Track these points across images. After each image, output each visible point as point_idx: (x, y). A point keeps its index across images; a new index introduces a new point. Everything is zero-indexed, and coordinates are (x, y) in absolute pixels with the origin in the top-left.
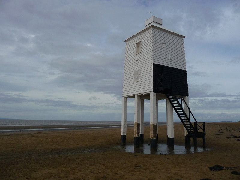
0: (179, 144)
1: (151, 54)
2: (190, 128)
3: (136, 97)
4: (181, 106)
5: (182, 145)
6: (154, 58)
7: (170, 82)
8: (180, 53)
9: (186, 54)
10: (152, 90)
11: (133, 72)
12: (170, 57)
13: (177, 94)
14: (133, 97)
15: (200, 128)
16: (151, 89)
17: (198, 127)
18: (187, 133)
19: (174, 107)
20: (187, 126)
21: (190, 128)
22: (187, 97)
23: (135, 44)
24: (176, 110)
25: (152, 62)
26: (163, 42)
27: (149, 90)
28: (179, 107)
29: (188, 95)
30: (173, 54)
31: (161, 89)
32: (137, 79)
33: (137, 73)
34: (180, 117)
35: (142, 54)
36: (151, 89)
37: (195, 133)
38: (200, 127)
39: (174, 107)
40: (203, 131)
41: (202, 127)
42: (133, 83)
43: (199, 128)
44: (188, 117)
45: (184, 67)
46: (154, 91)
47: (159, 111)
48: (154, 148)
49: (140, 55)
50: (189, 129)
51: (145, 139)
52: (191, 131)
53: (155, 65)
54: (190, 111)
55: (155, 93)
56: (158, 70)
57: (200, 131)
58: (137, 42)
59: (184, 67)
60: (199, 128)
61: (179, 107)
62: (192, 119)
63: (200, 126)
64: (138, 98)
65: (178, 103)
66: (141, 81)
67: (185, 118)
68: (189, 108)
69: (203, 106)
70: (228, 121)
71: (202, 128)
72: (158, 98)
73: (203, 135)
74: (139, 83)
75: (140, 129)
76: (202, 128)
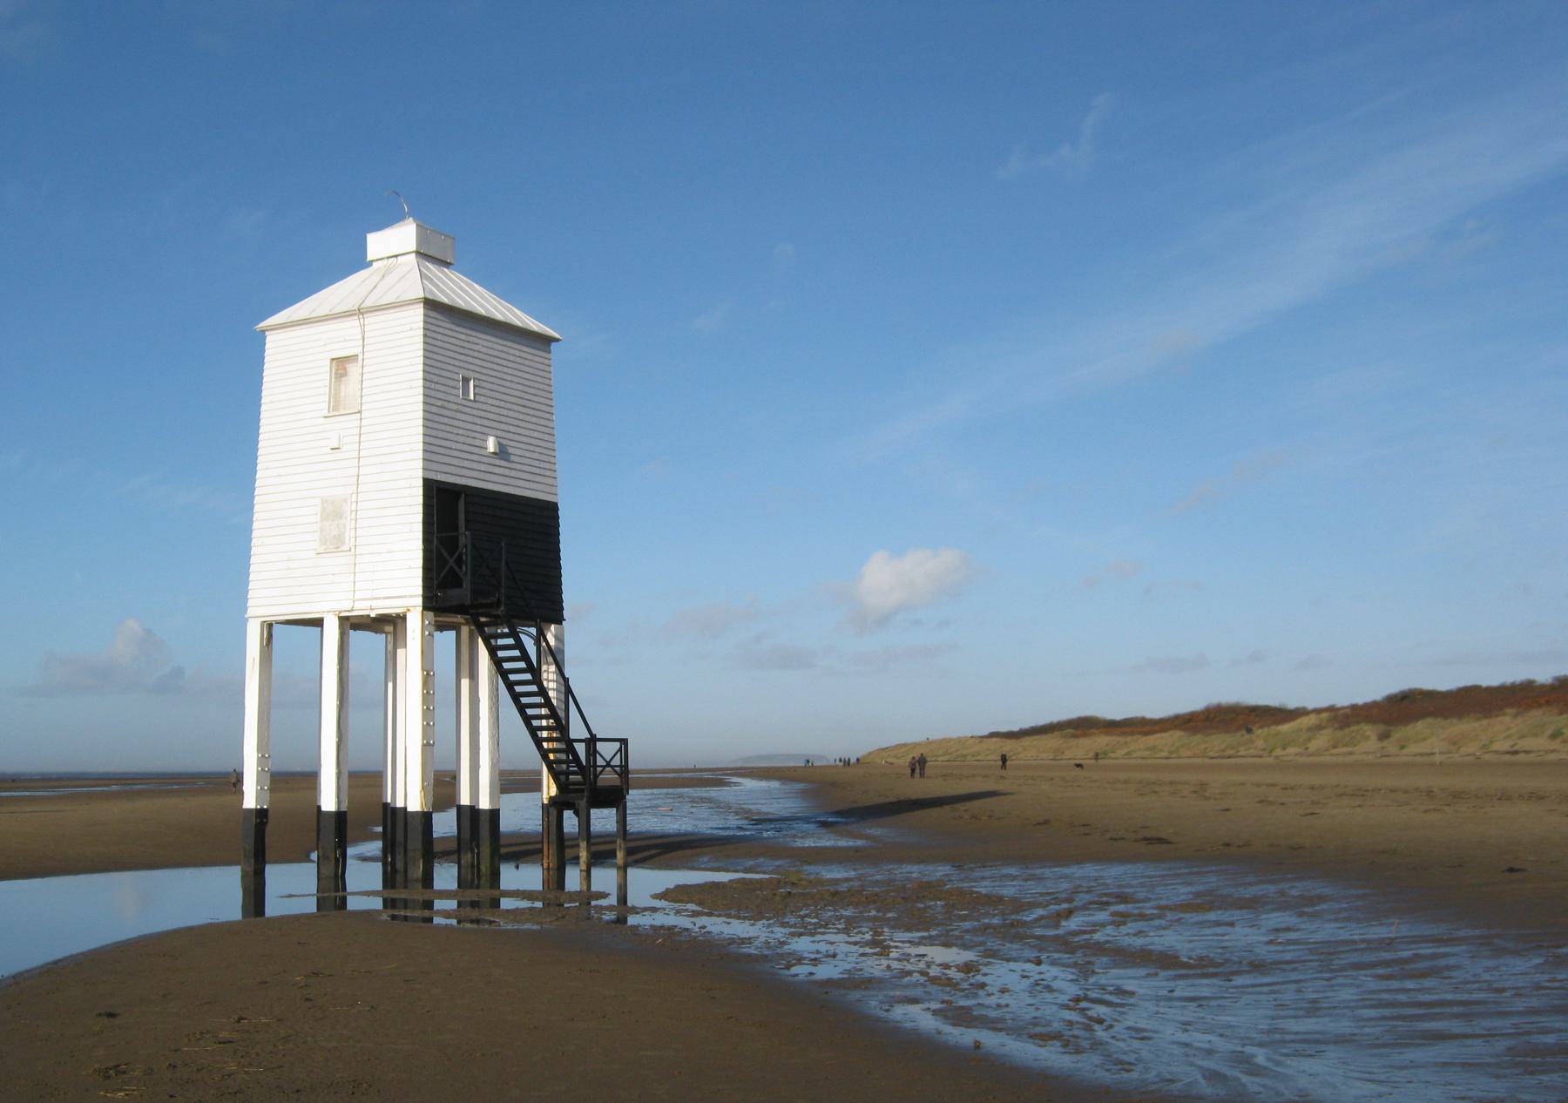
4: (537, 680)
17: (600, 761)
18: (554, 791)
28: (528, 676)
29: (558, 619)
31: (464, 594)
33: (333, 511)
40: (618, 782)
44: (562, 714)
46: (426, 608)
48: (480, 884)
53: (428, 484)
54: (568, 691)
55: (431, 614)
56: (446, 506)
57: (608, 778)
61: (528, 676)
62: (577, 730)
67: (545, 714)
70: (760, 757)
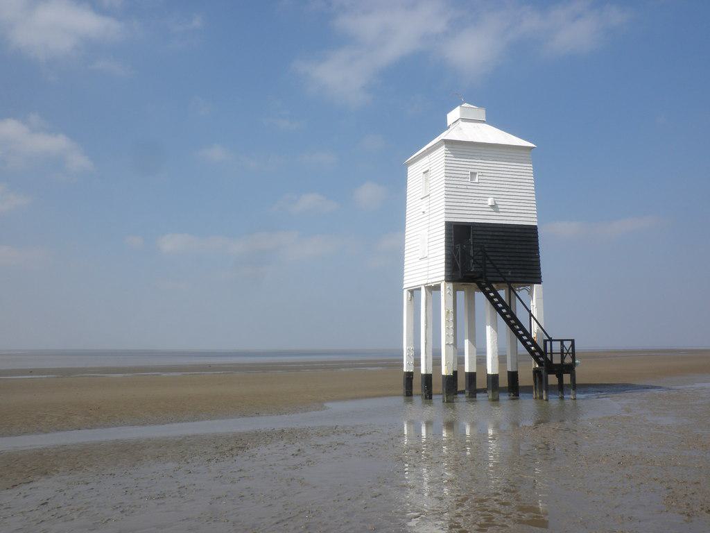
0: (568, 385)
1: (441, 201)
6: (448, 209)
10: (443, 278)
12: (490, 202)
13: (514, 282)
25: (444, 220)
26: (473, 171)
27: (436, 277)
30: (521, 184)
35: (431, 199)
41: (570, 351)
42: (418, 260)
46: (447, 281)
57: (568, 360)
66: (430, 256)
68: (530, 311)
73: (570, 368)
74: (427, 261)
75: (171, 374)
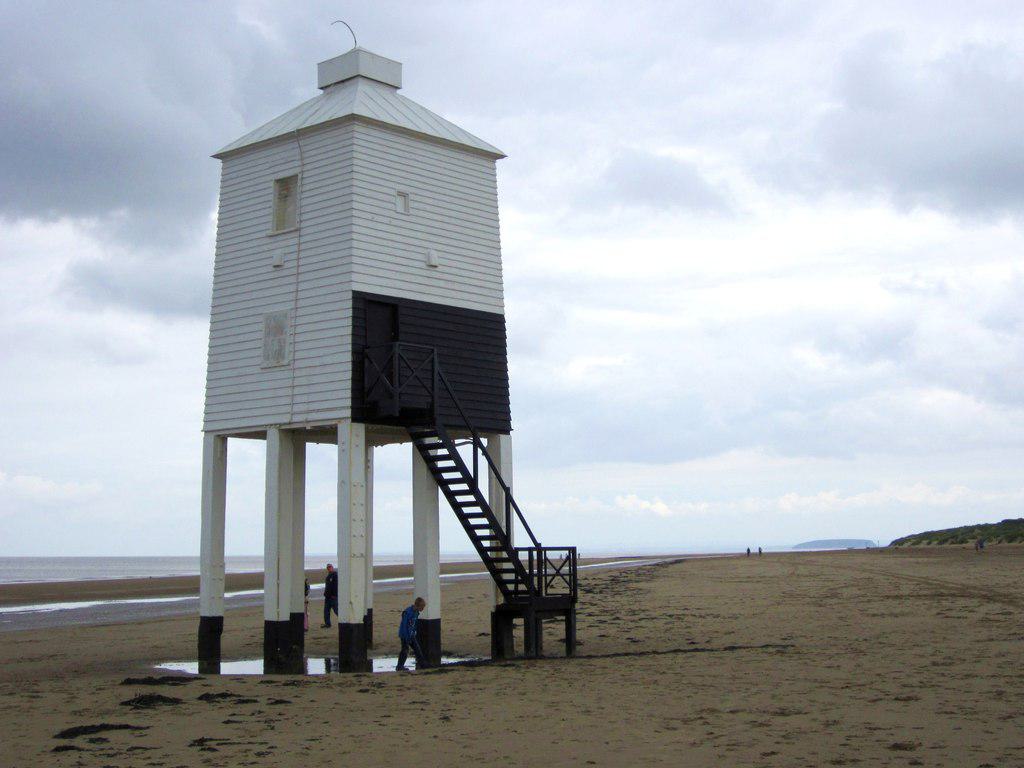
2: (512, 576)
3: (273, 434)
5: (233, 558)
7: (430, 374)
8: (460, 182)
9: (500, 210)
10: (348, 413)
11: (261, 319)
14: (260, 435)
15: (558, 573)
16: (343, 408)
19: (444, 484)
20: (498, 565)
21: (512, 576)
22: (503, 437)
23: (272, 184)
24: (450, 495)
32: (280, 354)
33: (276, 328)
34: (476, 540)
36: (343, 408)
37: (536, 601)
38: (558, 571)
39: (444, 484)
41: (566, 569)
42: (257, 370)
43: (554, 576)
44: (504, 530)
45: (493, 301)
46: (355, 419)
47: (382, 512)
49: (292, 240)
50: (510, 582)
51: (311, 637)
52: (516, 591)
57: (560, 588)
58: (281, 175)
59: (493, 301)
60: (554, 576)
62: (520, 539)
63: (558, 568)
64: (281, 445)
65: (460, 466)
67: (496, 547)
69: (575, 495)
71: (562, 576)
72: (372, 441)
76: (562, 576)
